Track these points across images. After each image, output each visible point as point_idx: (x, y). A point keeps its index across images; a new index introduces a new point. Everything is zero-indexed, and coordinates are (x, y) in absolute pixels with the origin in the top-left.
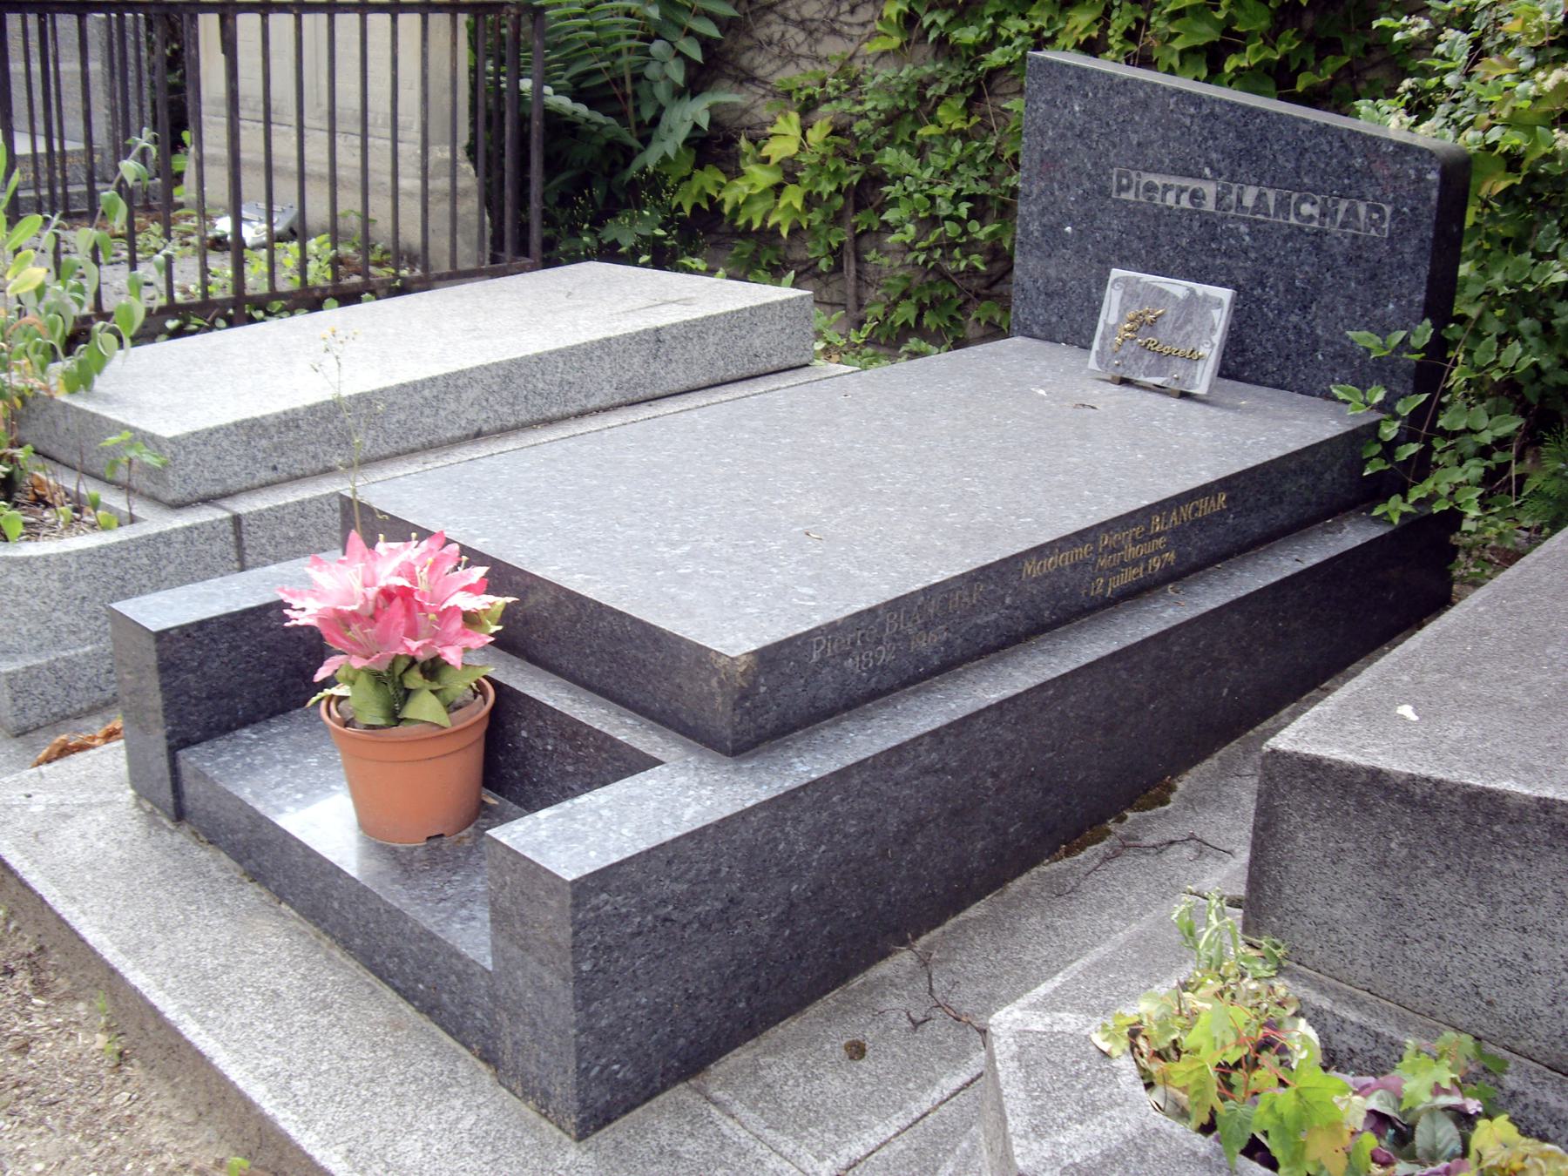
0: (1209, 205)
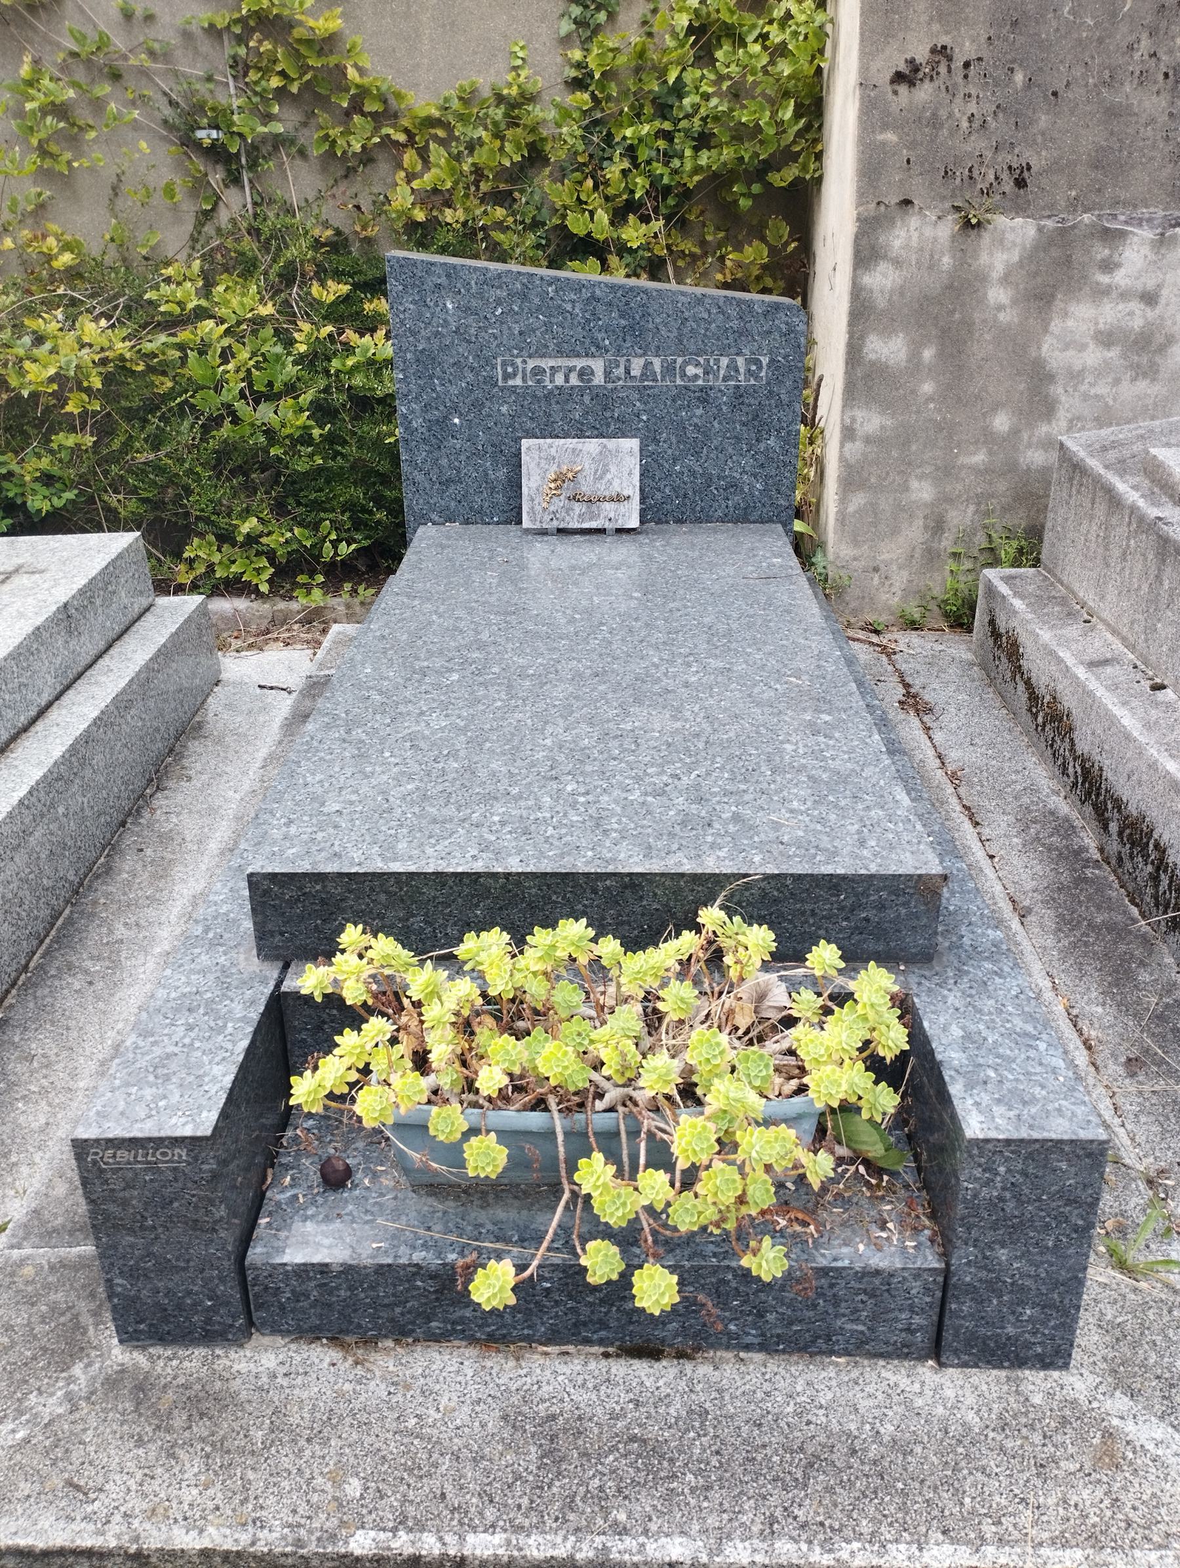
0: (599, 379)
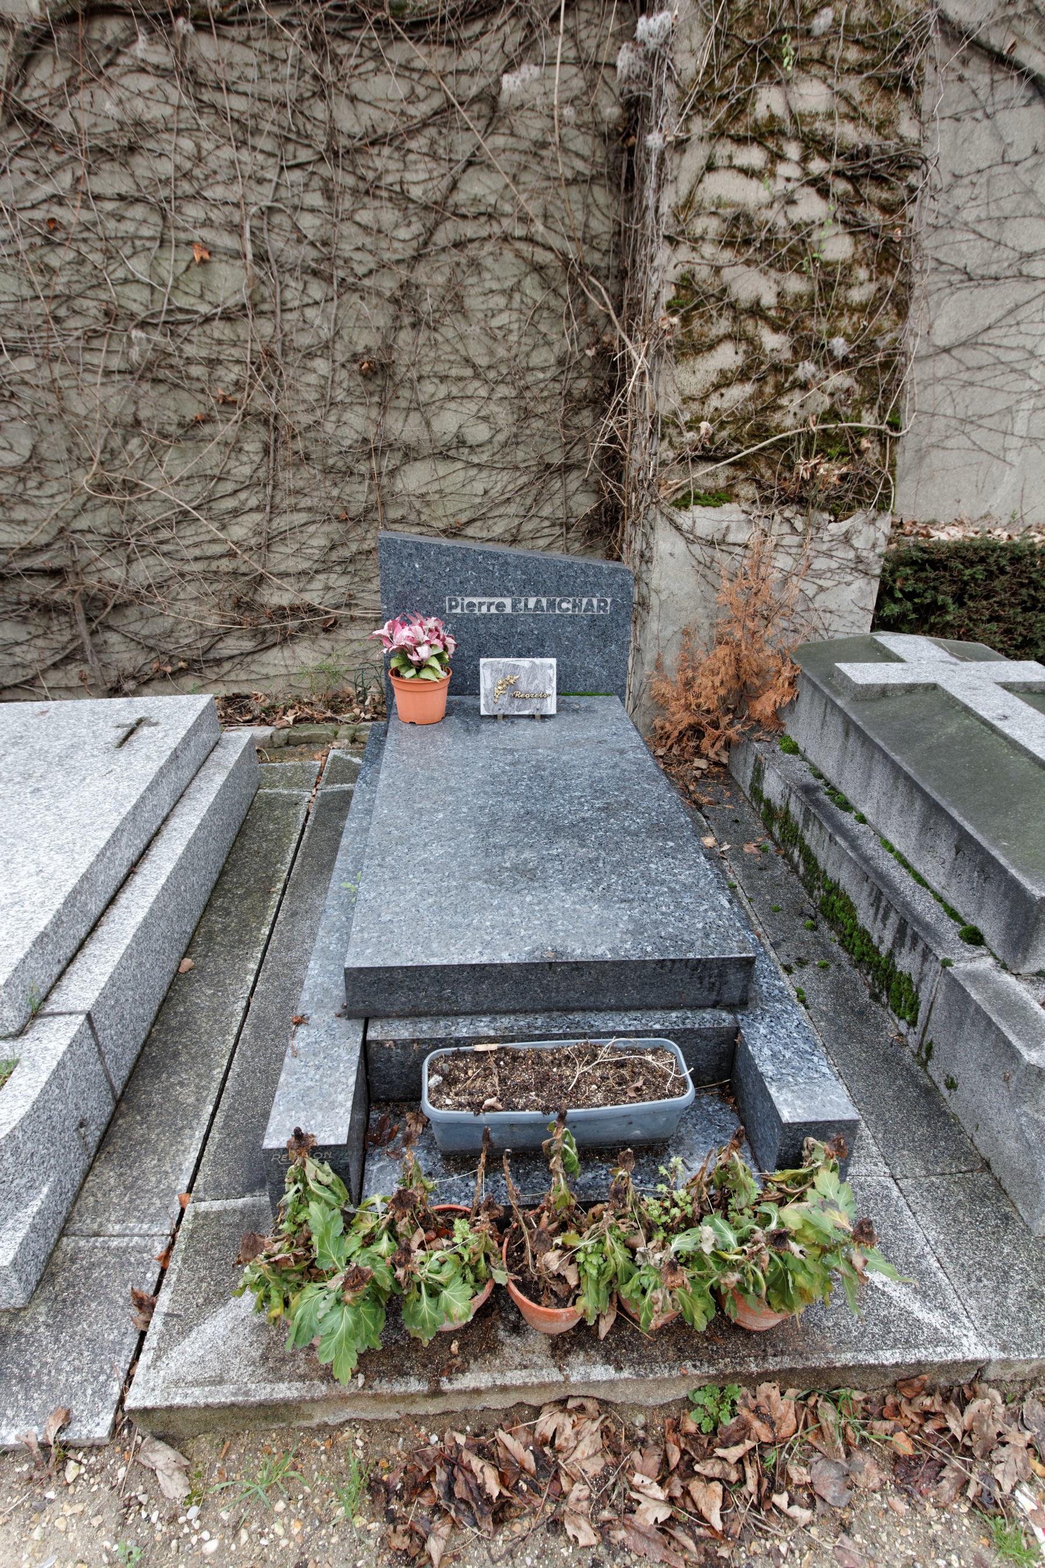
0: (508, 610)
